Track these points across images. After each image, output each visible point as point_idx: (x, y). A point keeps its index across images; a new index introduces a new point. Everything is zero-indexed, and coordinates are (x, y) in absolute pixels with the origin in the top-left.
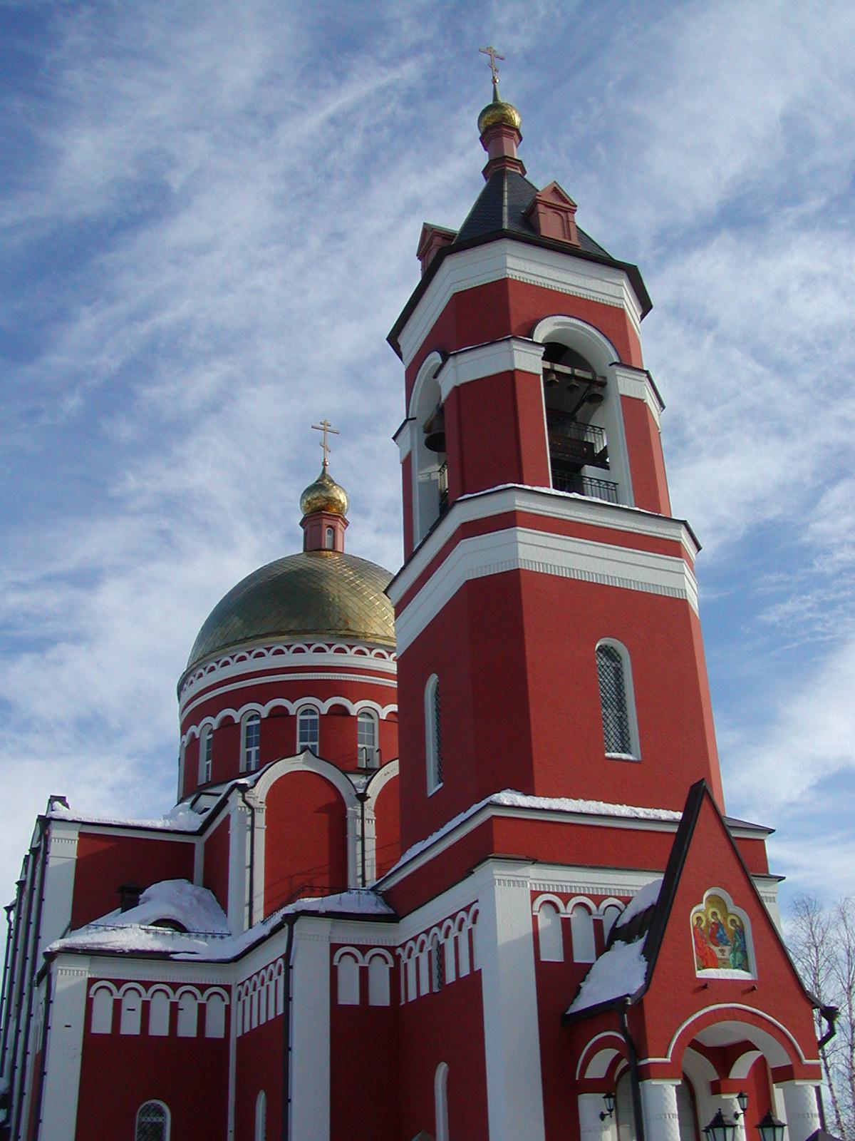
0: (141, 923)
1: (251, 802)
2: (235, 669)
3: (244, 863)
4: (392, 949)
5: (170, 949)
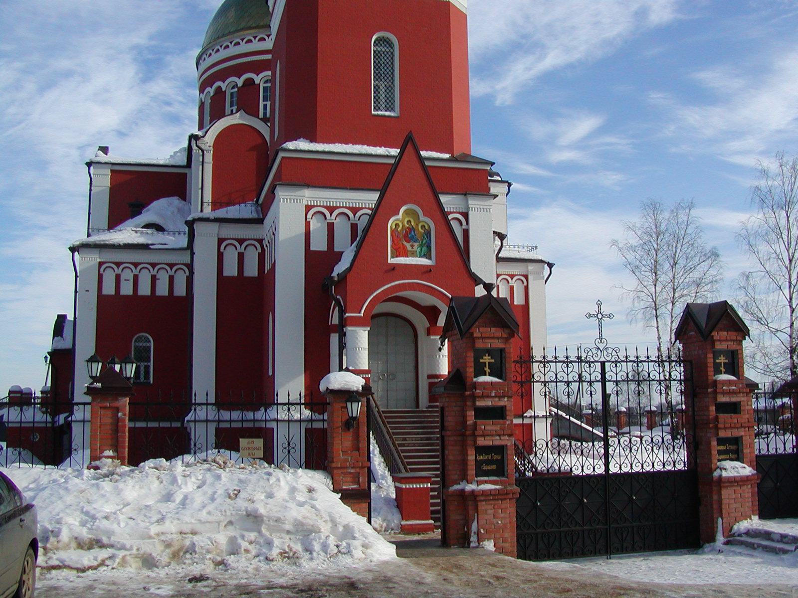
0: (136, 227)
1: (203, 147)
2: (233, 51)
3: (198, 186)
4: (260, 241)
5: (150, 242)
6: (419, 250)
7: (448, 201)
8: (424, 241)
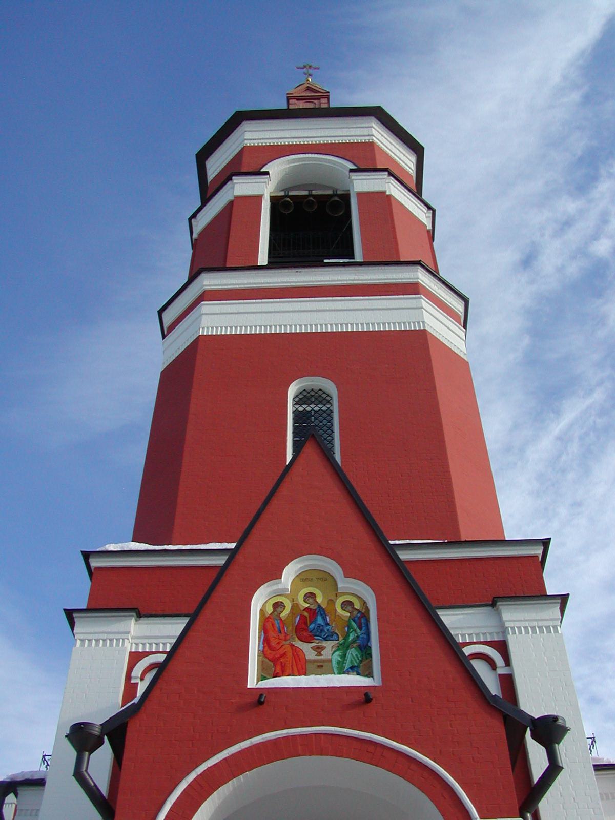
6: (336, 657)
7: (462, 623)
8: (351, 637)
